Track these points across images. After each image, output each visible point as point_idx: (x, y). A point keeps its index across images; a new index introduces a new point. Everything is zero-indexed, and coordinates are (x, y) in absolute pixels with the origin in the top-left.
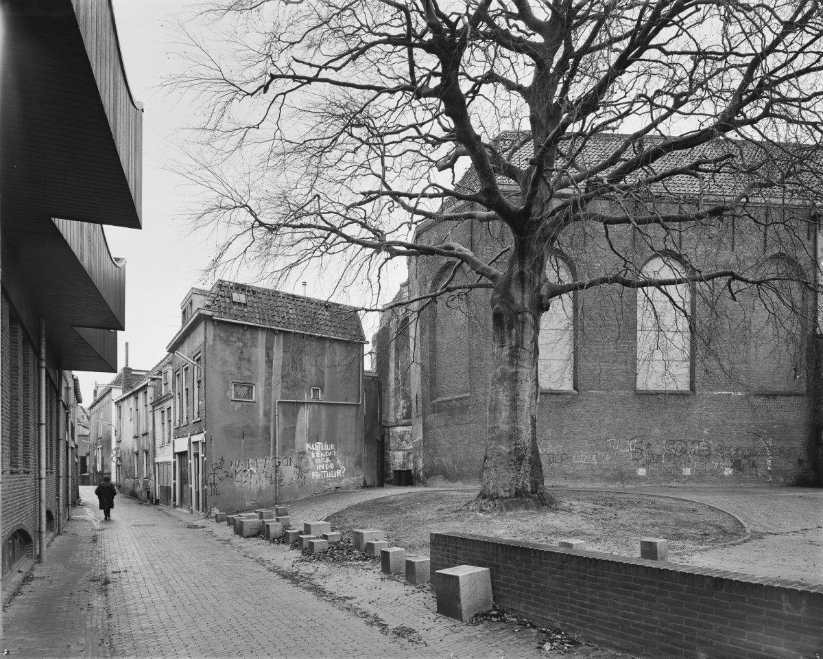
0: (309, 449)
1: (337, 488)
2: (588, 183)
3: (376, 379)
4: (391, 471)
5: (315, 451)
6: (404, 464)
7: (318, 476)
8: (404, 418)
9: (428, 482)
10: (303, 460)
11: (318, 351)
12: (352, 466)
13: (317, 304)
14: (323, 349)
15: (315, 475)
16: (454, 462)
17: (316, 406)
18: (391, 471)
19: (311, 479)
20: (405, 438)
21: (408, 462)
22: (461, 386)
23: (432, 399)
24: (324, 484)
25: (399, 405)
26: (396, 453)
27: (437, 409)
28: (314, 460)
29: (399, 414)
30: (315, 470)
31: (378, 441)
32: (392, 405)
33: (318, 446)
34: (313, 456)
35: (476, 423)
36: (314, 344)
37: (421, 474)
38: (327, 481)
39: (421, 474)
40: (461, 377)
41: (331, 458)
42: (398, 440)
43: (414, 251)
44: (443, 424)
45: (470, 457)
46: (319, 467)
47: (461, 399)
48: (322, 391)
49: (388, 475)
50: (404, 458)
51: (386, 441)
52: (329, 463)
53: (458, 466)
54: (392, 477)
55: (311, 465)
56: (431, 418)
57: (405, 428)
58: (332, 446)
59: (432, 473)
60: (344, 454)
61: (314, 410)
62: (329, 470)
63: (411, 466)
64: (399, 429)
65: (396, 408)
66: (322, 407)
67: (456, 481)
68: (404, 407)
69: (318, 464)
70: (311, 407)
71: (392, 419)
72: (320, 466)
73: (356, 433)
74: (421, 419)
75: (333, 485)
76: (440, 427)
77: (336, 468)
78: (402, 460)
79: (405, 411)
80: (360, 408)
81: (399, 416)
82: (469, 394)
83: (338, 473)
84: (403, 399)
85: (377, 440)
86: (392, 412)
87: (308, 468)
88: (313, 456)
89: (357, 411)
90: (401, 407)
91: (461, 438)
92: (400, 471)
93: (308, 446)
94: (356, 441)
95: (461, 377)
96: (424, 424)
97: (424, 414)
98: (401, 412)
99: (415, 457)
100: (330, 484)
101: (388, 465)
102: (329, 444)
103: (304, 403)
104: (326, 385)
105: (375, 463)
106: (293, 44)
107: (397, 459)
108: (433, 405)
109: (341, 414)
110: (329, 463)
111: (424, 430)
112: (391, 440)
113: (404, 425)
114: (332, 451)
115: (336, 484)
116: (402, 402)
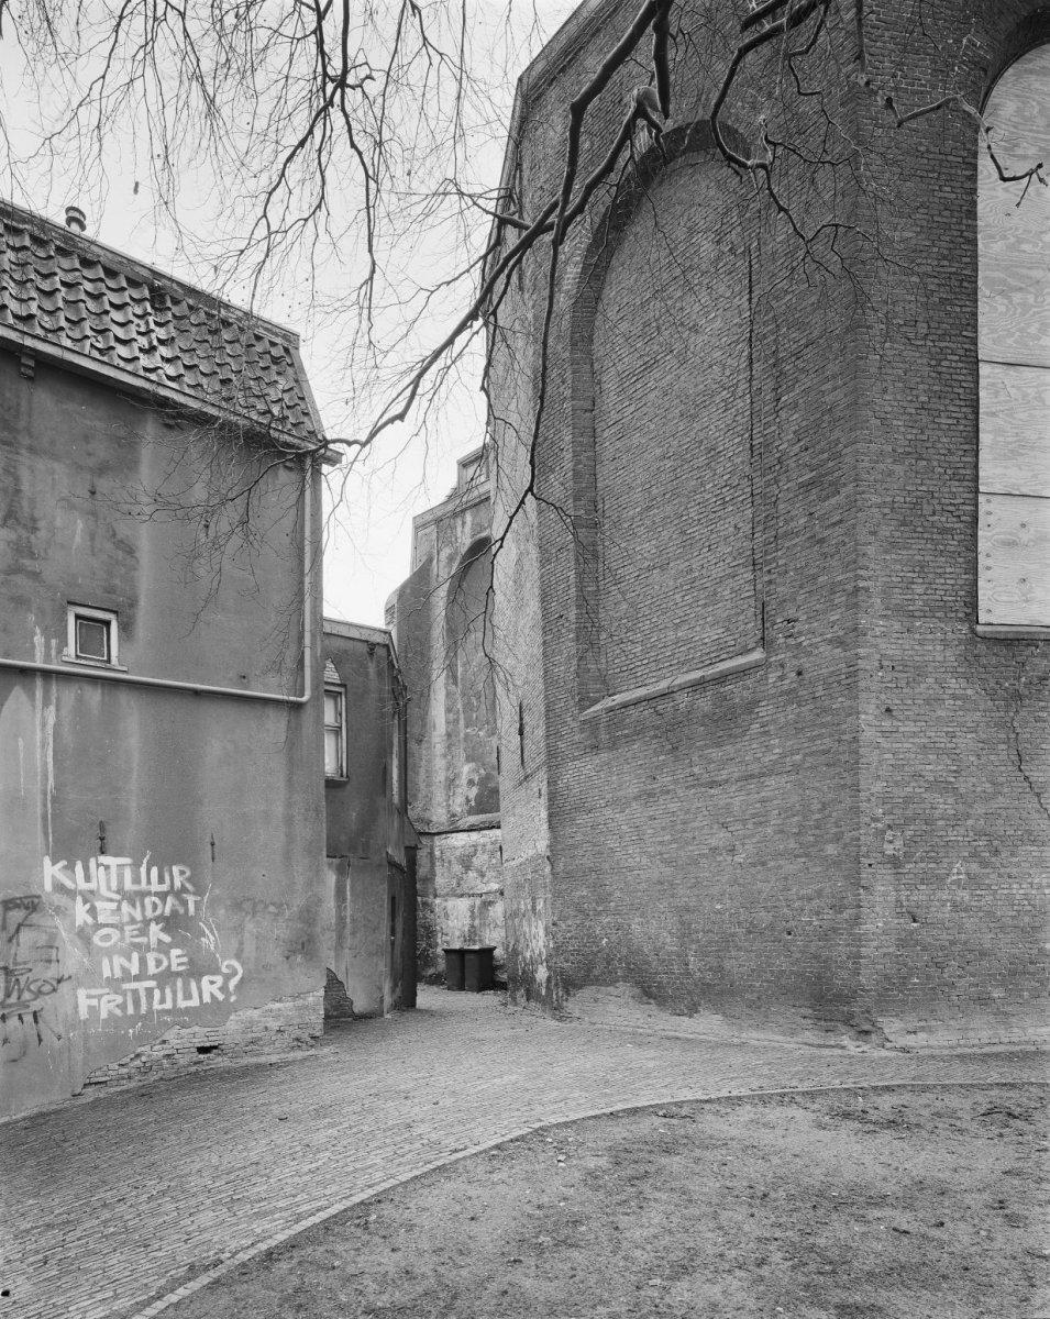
0: (60, 888)
1: (202, 1050)
2: (213, 1202)
3: (381, 652)
4: (439, 951)
5: (89, 897)
6: (473, 933)
7: (108, 1005)
8: (470, 813)
9: (572, 1006)
10: (26, 936)
11: (102, 450)
12: (274, 955)
13: (87, 263)
14: (129, 444)
15: (92, 1003)
16: (685, 933)
17: (94, 696)
18: (439, 951)
19: (74, 1023)
20: (476, 861)
21: (483, 925)
22: (713, 634)
23: (585, 701)
24: (141, 1039)
25: (457, 776)
26: (451, 903)
27: (607, 735)
28: (84, 936)
29: (460, 800)
30: (91, 977)
31: (392, 864)
32: (440, 776)
33: (109, 873)
34: (81, 913)
35: (797, 768)
36: (91, 417)
37: (542, 974)
38: (152, 1025)
39: (542, 974)
40: (714, 597)
41: (171, 923)
42: (457, 868)
43: (495, 215)
44: (633, 790)
45: (764, 918)
46: (110, 968)
47: (721, 679)
48: (126, 628)
49: (429, 961)
50: (473, 917)
51: (422, 872)
52: (163, 948)
53: (702, 953)
54: (442, 965)
55: (72, 958)
56: (581, 772)
57: (474, 836)
58: (178, 875)
59: (577, 975)
60: (237, 906)
61: (80, 707)
62: (166, 978)
63: (493, 938)
64: (460, 840)
65: (451, 783)
66: (124, 698)
67: (693, 1010)
68: (471, 782)
69: (109, 953)
70: (69, 694)
71: (439, 816)
72: (118, 961)
73: (289, 820)
74: (540, 782)
75: (183, 1039)
76: (620, 804)
77: (196, 970)
78: (468, 921)
79: (474, 791)
80: (308, 716)
81: (458, 805)
82: (757, 655)
83: (210, 987)
84: (469, 759)
85: (377, 838)
86: (439, 796)
87: (52, 972)
88: (81, 913)
89: (294, 730)
90: (464, 781)
91: (720, 838)
92: (461, 953)
93: (51, 871)
94: (287, 856)
95: (714, 597)
96: (552, 798)
97: (553, 759)
98: (466, 792)
99: (512, 915)
100: (170, 1035)
101: (430, 933)
102: (162, 862)
103: (26, 673)
104: (143, 602)
105: (383, 935)
106: (242, 251)
107: (453, 921)
108: (592, 725)
109: (221, 741)
110: (163, 948)
111: (555, 818)
112: (438, 870)
113: (471, 829)
114: (179, 894)
115: (201, 1035)
116: (466, 769)
